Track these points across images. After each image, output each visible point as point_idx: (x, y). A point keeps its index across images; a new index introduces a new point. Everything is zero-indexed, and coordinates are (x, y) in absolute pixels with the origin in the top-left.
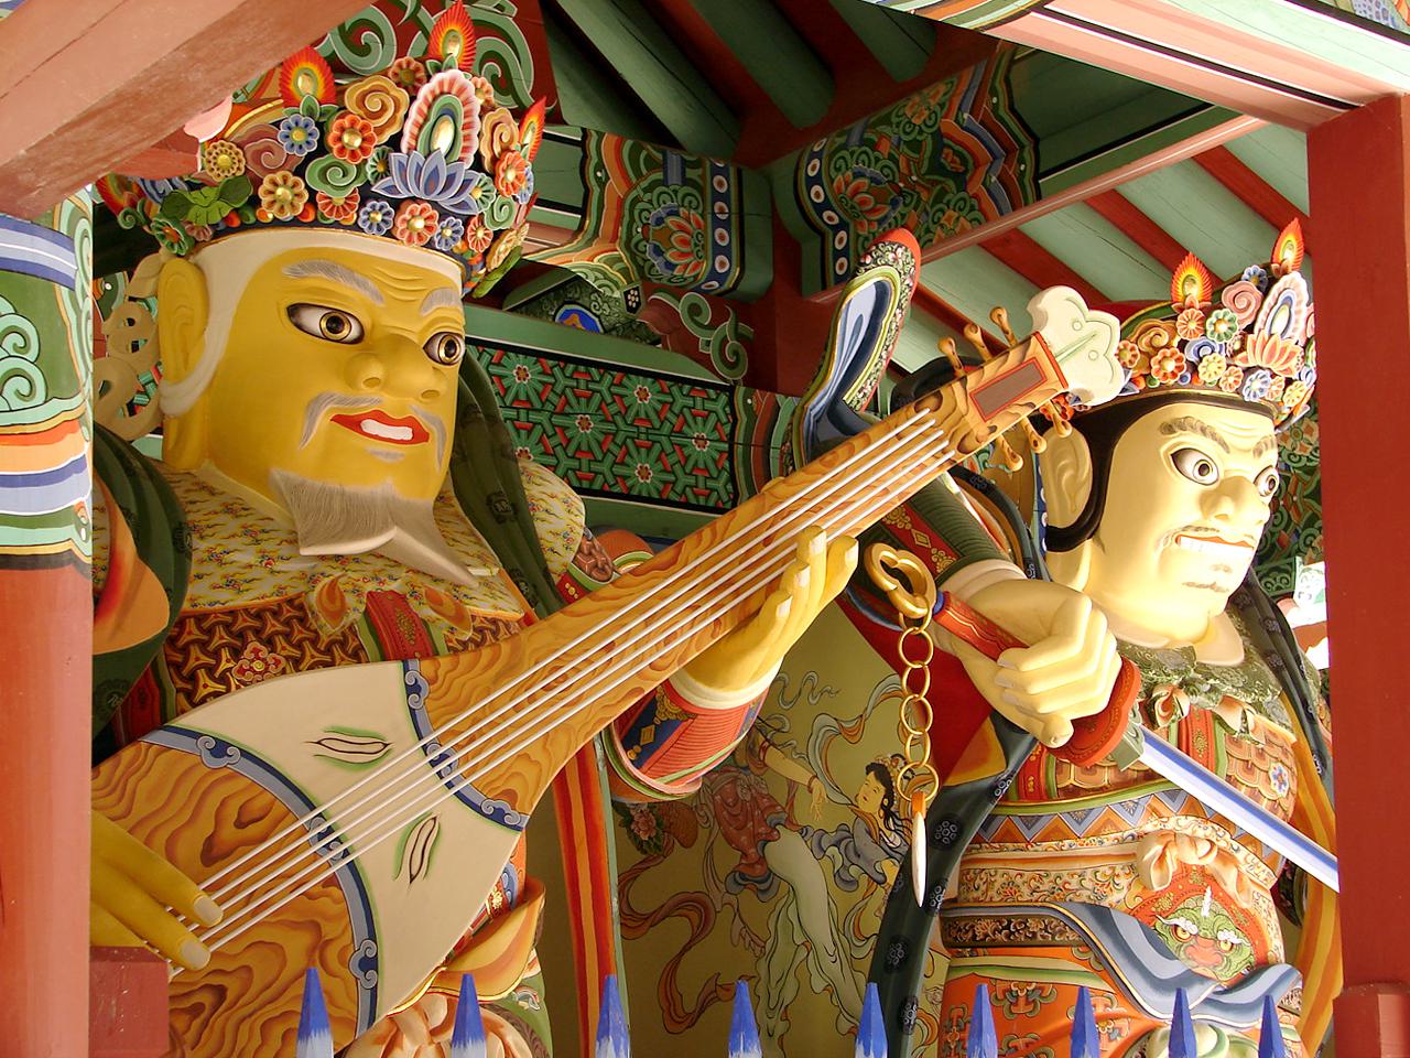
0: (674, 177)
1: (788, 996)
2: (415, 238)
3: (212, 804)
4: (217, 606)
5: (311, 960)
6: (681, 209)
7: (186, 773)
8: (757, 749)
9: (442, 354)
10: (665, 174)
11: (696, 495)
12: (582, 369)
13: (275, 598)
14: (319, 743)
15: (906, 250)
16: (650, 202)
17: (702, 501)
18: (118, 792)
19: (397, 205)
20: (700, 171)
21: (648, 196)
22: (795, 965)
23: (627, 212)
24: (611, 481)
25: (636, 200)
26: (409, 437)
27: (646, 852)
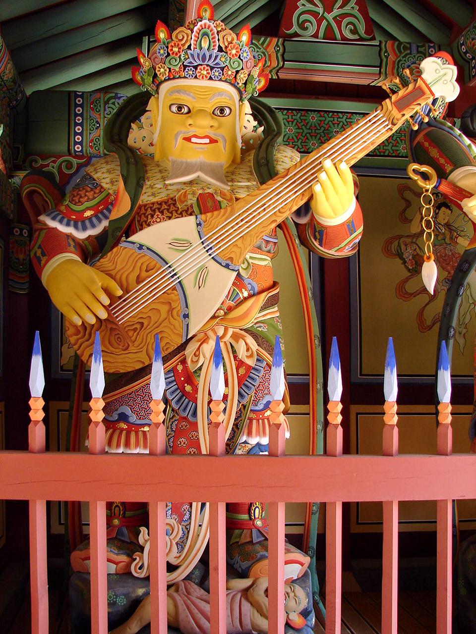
0: (414, 51)
1: (467, 320)
2: (205, 77)
3: (139, 264)
4: (149, 202)
5: (168, 315)
6: (417, 62)
7: (131, 255)
8: (454, 237)
9: (219, 114)
10: (411, 52)
11: (380, 152)
12: (336, 114)
13: (166, 198)
14: (170, 244)
15: (443, 59)
16: (405, 61)
17: (382, 154)
18: (112, 262)
19: (196, 67)
20: (424, 48)
21: (404, 59)
22: (470, 310)
23: (396, 65)
24: (392, 152)
25: (400, 60)
26: (209, 142)
27: (411, 272)
